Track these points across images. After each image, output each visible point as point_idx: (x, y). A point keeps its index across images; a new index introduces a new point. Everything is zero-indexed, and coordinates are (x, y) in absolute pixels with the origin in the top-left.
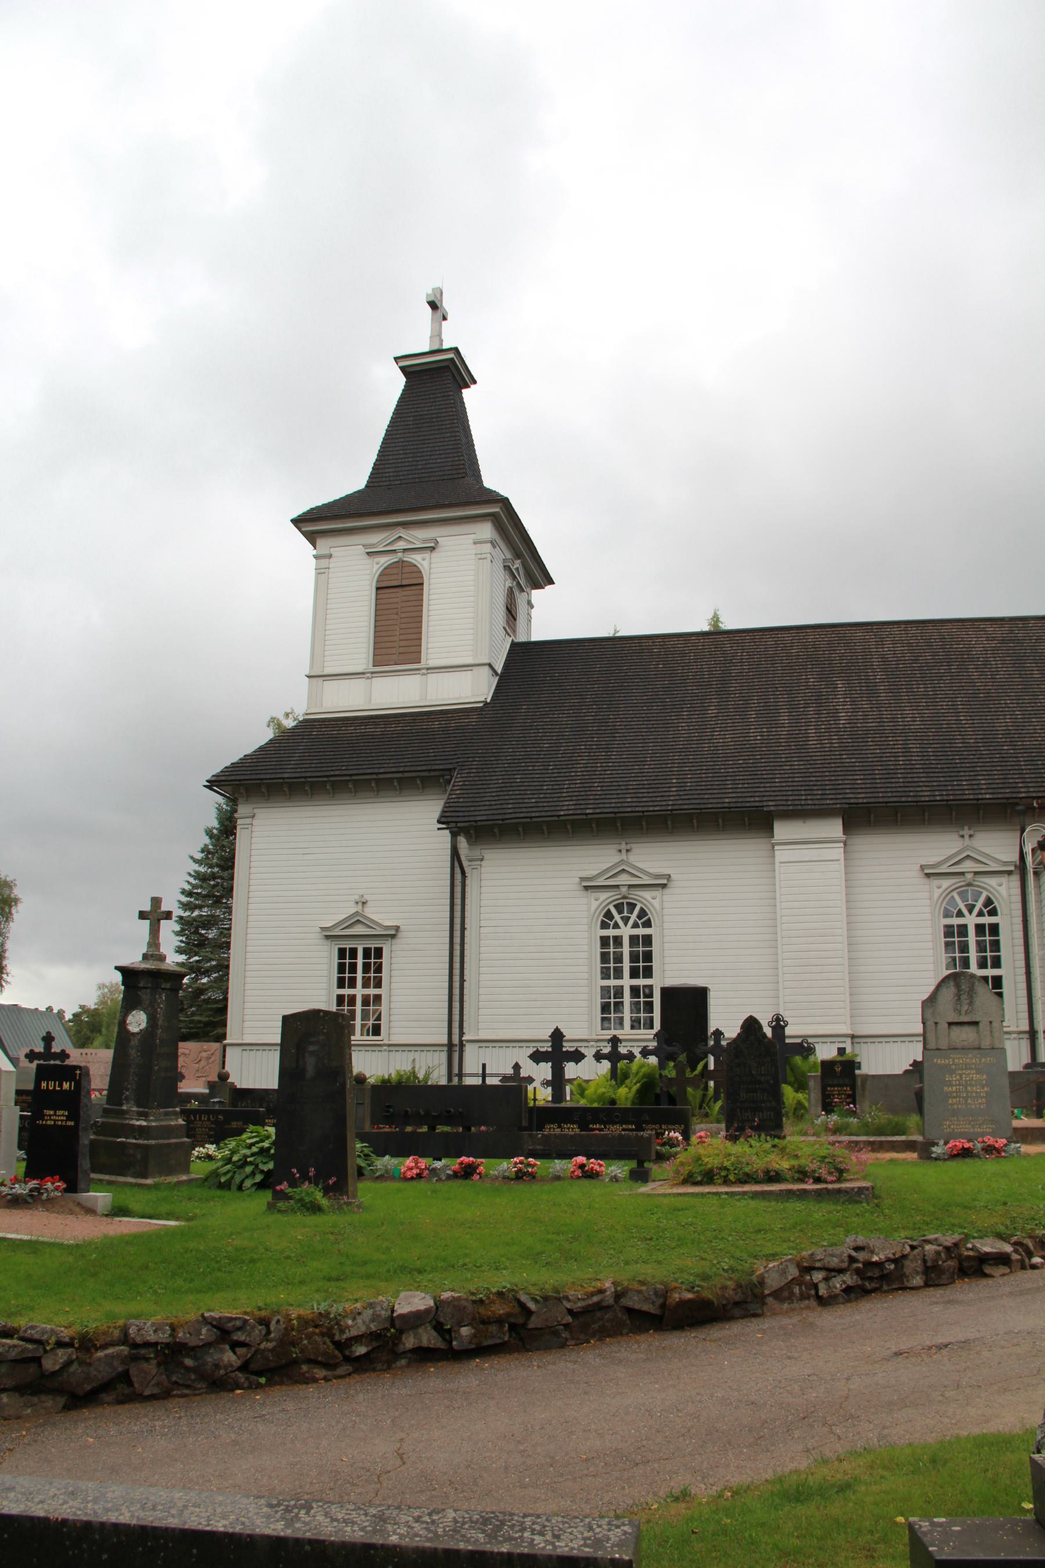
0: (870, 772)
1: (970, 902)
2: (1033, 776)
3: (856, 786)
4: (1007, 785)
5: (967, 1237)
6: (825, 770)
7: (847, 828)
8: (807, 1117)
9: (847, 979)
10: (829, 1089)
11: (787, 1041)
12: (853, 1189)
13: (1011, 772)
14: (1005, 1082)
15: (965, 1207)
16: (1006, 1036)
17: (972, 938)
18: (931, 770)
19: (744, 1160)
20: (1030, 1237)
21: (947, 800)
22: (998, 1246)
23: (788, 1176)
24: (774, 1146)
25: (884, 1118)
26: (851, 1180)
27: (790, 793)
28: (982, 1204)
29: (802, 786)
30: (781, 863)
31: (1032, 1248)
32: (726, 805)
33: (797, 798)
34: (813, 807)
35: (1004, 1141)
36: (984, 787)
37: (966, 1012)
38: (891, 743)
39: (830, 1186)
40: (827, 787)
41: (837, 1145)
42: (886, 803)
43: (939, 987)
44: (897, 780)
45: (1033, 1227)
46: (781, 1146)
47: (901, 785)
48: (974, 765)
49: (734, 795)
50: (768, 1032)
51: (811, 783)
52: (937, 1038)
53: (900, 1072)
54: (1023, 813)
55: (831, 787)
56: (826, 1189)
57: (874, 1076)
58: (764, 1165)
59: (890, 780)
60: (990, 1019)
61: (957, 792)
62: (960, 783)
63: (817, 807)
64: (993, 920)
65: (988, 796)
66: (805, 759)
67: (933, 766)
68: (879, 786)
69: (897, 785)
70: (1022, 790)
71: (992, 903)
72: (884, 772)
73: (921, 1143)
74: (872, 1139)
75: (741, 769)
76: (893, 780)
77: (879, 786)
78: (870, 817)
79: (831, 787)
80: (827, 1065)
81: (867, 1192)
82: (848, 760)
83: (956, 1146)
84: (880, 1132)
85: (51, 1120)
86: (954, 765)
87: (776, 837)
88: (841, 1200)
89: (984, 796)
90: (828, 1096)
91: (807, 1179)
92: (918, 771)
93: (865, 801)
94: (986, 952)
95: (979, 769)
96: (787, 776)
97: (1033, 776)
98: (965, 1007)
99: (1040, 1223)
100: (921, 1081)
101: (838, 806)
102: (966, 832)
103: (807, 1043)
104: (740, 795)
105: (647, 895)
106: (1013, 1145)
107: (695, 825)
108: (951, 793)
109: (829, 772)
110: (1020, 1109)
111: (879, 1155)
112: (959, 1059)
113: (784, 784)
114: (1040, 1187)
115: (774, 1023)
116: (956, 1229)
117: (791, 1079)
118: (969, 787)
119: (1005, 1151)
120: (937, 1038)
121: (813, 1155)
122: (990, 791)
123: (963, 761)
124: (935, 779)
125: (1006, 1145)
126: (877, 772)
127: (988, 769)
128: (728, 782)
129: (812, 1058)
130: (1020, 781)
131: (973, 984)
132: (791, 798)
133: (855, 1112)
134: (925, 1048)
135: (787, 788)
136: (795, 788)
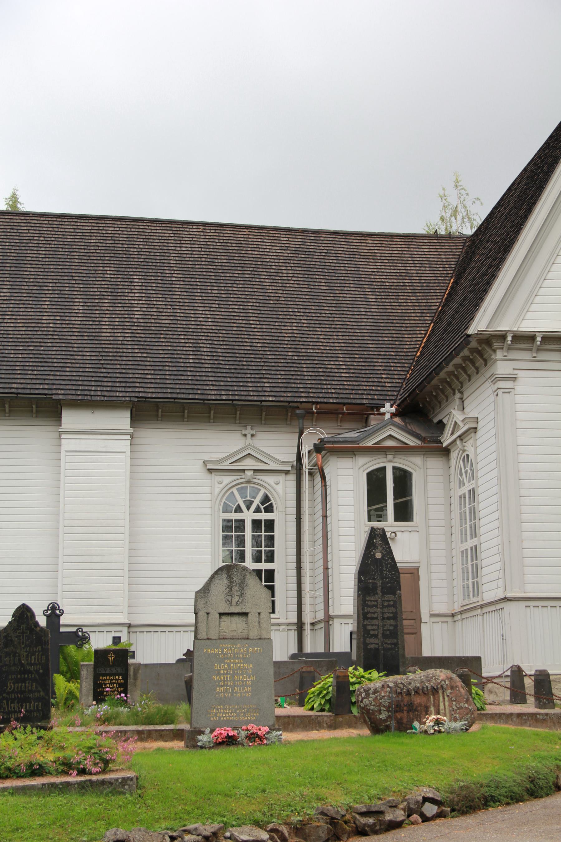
0: (161, 368)
1: (248, 498)
2: (313, 382)
3: (146, 381)
4: (289, 389)
5: (226, 826)
6: (116, 362)
7: (135, 420)
8: (78, 707)
9: (126, 569)
10: (101, 678)
11: (62, 630)
12: (117, 780)
13: (294, 377)
14: (271, 671)
15: (226, 795)
16: (273, 628)
17: (248, 533)
18: (219, 370)
19: (7, 754)
20: (286, 824)
21: (233, 400)
22: (255, 834)
23: (52, 769)
24: (40, 738)
25: (153, 707)
26: (117, 770)
27: (80, 383)
28: (242, 792)
29: (93, 376)
30: (67, 452)
31: (287, 835)
32: (13, 391)
33: (86, 388)
34: (102, 398)
35: (267, 729)
36: (268, 389)
37: (237, 603)
38: (183, 341)
39: (94, 778)
40: (118, 380)
41: (104, 734)
42: (175, 399)
43: (212, 578)
44: (186, 378)
45: (289, 813)
46: (47, 738)
47: (190, 382)
48: (260, 368)
49: (22, 381)
50: (42, 621)
51: (102, 375)
52: (208, 628)
53: (173, 661)
54: (302, 417)
55: (121, 380)
56: (90, 780)
57: (146, 665)
58: (28, 758)
59: (179, 377)
60: (259, 611)
61: (242, 393)
62: (245, 384)
63: (106, 399)
64: (269, 516)
65: (271, 399)
66: (97, 350)
67: (221, 366)
68: (168, 382)
69: (186, 382)
70: (303, 395)
71: (270, 500)
72: (174, 369)
73: (188, 731)
74: (141, 728)
75: (31, 356)
76: (183, 378)
77: (168, 382)
78: (157, 411)
79: (121, 380)
80: (101, 655)
81: (131, 783)
82: (140, 355)
83: (221, 734)
84: (149, 721)
86: (241, 367)
87: (63, 426)
88: (105, 792)
89: (267, 399)
90: (100, 686)
91: (71, 771)
92: (207, 370)
93: (154, 396)
94: (261, 547)
95: (264, 372)
96: (78, 365)
97: (313, 382)
98: (236, 599)
99: (296, 809)
100: (192, 671)
101: (127, 399)
102: (249, 431)
103: (82, 632)
104: (28, 381)
106: (275, 733)
107: (7, 410)
108: (236, 393)
109: (121, 365)
110: (284, 698)
111: (147, 745)
112: (227, 648)
113: (74, 374)
114: (297, 773)
115: (49, 612)
116: (216, 817)
117: (63, 668)
118: (254, 389)
119: (266, 738)
120: (208, 628)
121: (79, 745)
122: (273, 394)
123: (250, 363)
124: (223, 379)
125: (268, 733)
126: (167, 368)
127: (273, 372)
128: (17, 368)
129: (86, 647)
130: (301, 386)
131: (245, 576)
132: (81, 388)
133: (126, 701)
134: (196, 637)
135: (77, 378)
136: (86, 378)
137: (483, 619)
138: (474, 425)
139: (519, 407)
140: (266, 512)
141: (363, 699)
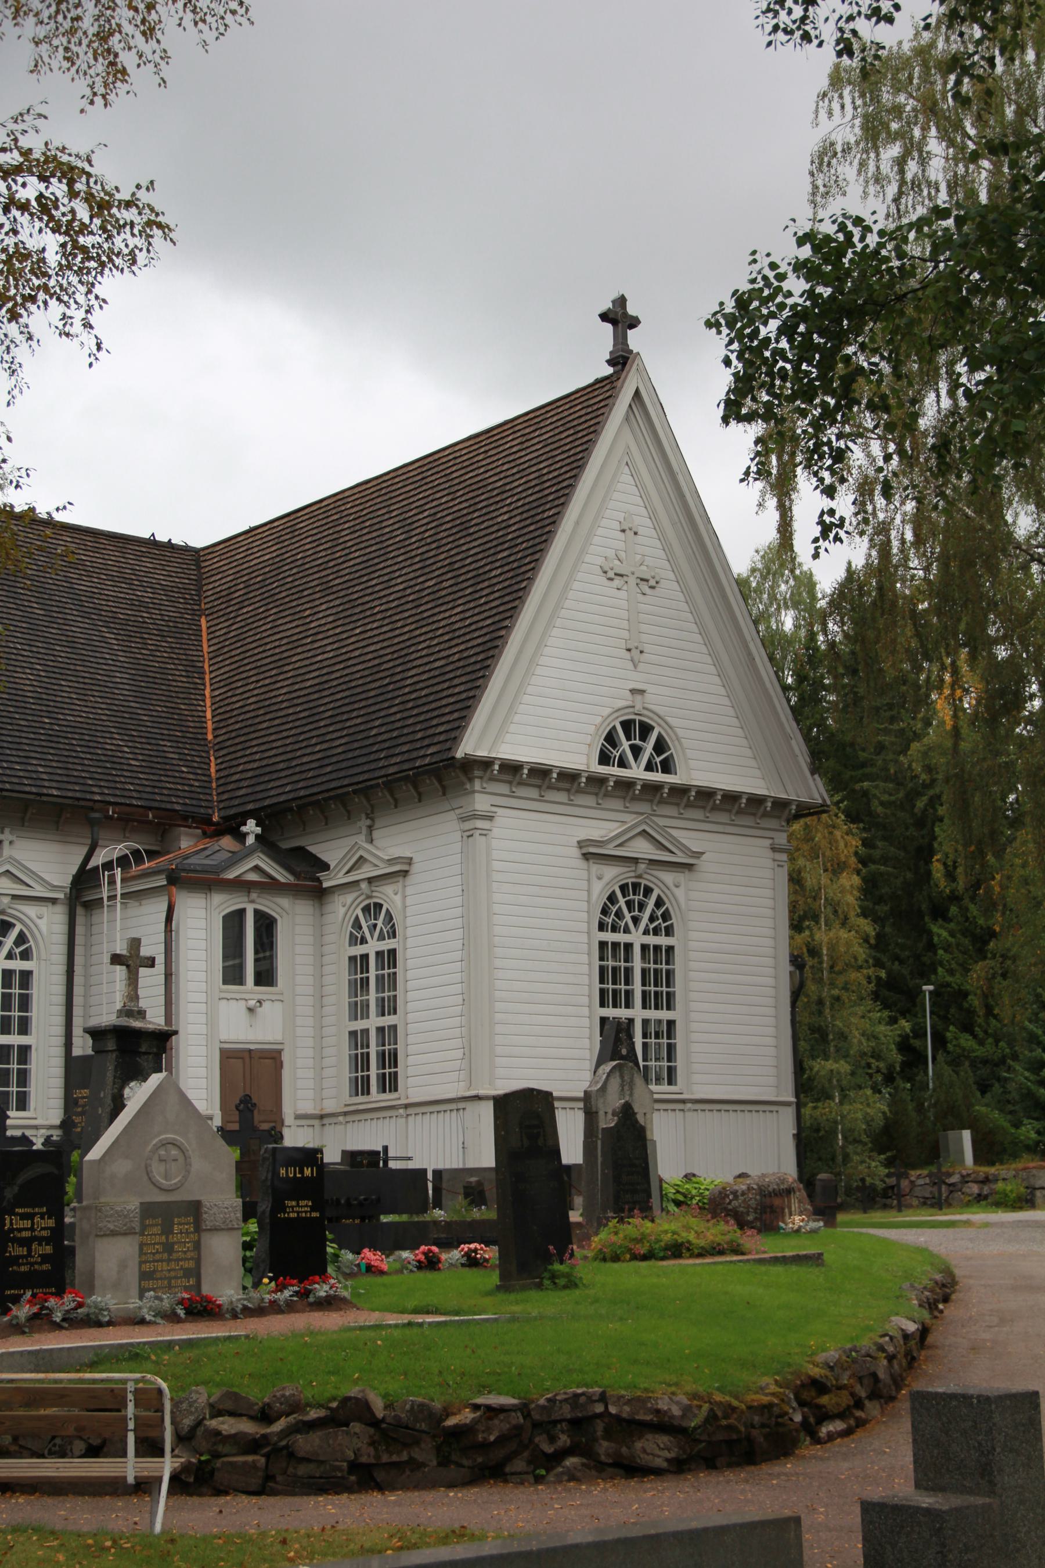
85: (293, 1212)
89: (50, 792)
105: (668, 877)
137: (407, 1122)
138: (405, 867)
139: (495, 854)
140: (21, 959)
141: (731, 1201)
